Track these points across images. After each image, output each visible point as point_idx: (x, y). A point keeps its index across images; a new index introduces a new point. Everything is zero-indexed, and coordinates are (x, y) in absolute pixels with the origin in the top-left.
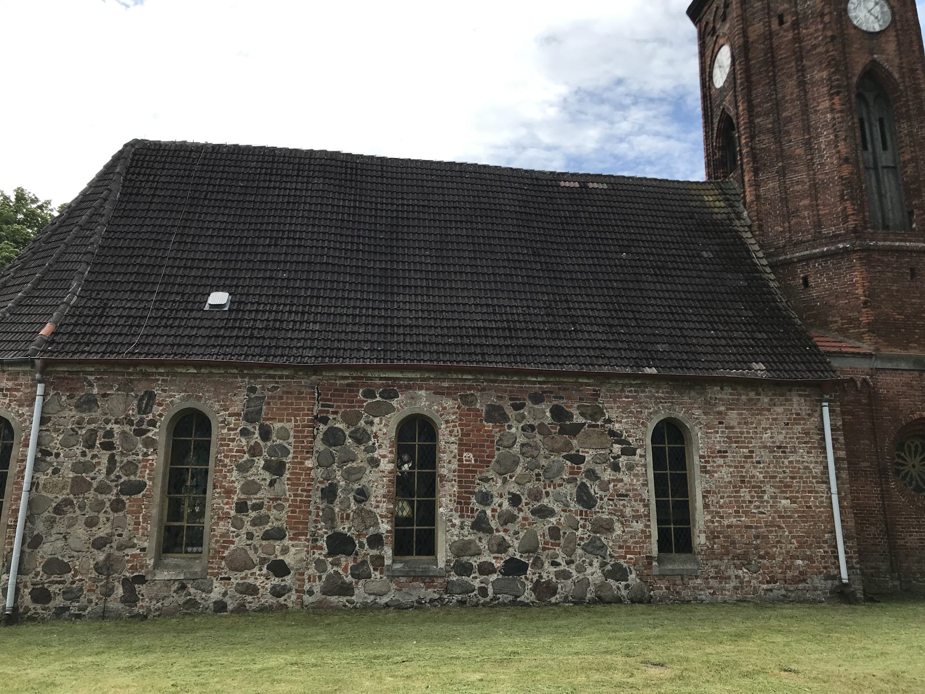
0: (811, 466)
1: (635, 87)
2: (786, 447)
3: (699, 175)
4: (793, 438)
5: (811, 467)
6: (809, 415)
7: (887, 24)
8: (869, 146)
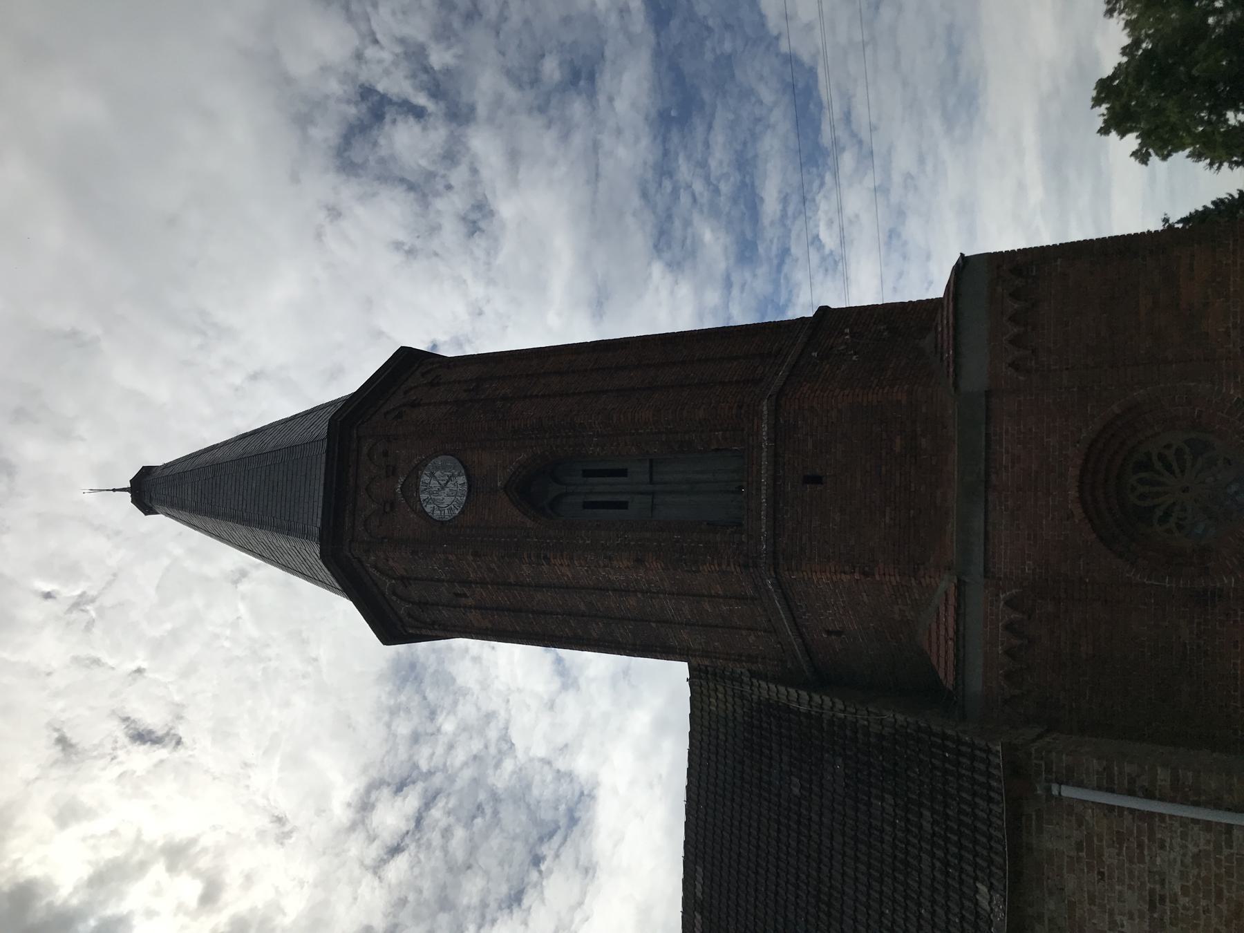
0: (1192, 849)
1: (650, 175)
2: (1152, 892)
3: (680, 670)
4: (1131, 872)
5: (1195, 850)
6: (1080, 825)
7: (458, 464)
8: (623, 498)
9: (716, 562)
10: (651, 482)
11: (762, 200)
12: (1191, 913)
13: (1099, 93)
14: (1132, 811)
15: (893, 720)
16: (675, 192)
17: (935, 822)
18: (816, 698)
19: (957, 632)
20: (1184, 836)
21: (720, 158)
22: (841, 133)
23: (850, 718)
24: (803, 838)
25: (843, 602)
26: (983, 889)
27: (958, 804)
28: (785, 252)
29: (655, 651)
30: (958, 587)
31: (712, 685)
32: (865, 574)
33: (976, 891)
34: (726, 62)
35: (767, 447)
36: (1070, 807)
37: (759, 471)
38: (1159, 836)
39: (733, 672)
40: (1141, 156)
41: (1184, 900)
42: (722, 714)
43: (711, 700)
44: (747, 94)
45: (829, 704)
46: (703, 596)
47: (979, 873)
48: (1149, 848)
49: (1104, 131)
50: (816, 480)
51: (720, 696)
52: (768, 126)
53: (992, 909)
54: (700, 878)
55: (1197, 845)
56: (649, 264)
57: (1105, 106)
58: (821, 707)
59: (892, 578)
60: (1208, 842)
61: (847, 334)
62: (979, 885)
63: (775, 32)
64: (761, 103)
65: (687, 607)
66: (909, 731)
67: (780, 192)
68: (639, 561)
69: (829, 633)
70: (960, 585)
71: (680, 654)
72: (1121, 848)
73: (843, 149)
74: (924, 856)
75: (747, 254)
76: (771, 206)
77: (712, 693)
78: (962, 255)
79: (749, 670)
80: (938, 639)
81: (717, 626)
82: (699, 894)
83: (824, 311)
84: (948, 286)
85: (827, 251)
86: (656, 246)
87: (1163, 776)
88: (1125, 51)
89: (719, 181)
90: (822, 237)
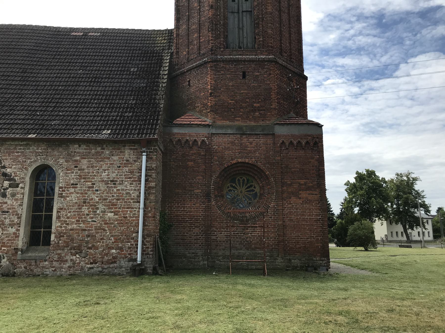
0: (131, 192)
1: (359, 11)
2: (117, 181)
5: (131, 193)
9: (213, 38)
10: (243, 12)
11: (344, 58)
12: (112, 192)
13: (370, 171)
14: (141, 175)
15: (161, 103)
16: (351, 22)
17: (128, 117)
18: (166, 77)
19: (192, 124)
20: (135, 190)
21: (362, 40)
22: (366, 87)
23: (160, 89)
24: (116, 72)
25: (200, 86)
26: (109, 132)
27: (135, 124)
28: (323, 67)
29: (177, 15)
30: (208, 125)
31: (166, 38)
32: (211, 94)
33: (108, 130)
34: (400, 42)
35: (256, 58)
36: (139, 158)
37: (247, 55)
38: (134, 183)
39: (172, 46)
40: (347, 183)
41: (115, 190)
42: (156, 42)
43: (161, 38)
44: (386, 51)
45: (164, 82)
46: (200, 34)
47: (114, 130)
48: (130, 180)
49: (357, 173)
50: (244, 76)
51: (163, 41)
52: (372, 60)
53: (103, 134)
54: (96, 34)
55: (133, 193)
56: (323, 12)
57: (366, 173)
58: (163, 78)
59: (210, 103)
60: (134, 196)
61: (297, 87)
62: (110, 130)
63: (409, 61)
64: (382, 57)
65: (195, 27)
66: (158, 108)
67: (346, 64)
68: (212, 7)
69: (189, 81)
70: (208, 126)
71: (177, 25)
72: (129, 172)
73: (360, 87)
74: (116, 113)
75: (324, 52)
76: (341, 61)
77: (163, 38)
78: (323, 126)
79: (173, 52)
80: (190, 118)
81: (188, 39)
82: (90, 34)
83: (306, 78)
84: (312, 121)
85: (324, 83)
86: (329, 15)
87: (153, 184)
88: (383, 180)
89: (353, 40)
90: (329, 80)
